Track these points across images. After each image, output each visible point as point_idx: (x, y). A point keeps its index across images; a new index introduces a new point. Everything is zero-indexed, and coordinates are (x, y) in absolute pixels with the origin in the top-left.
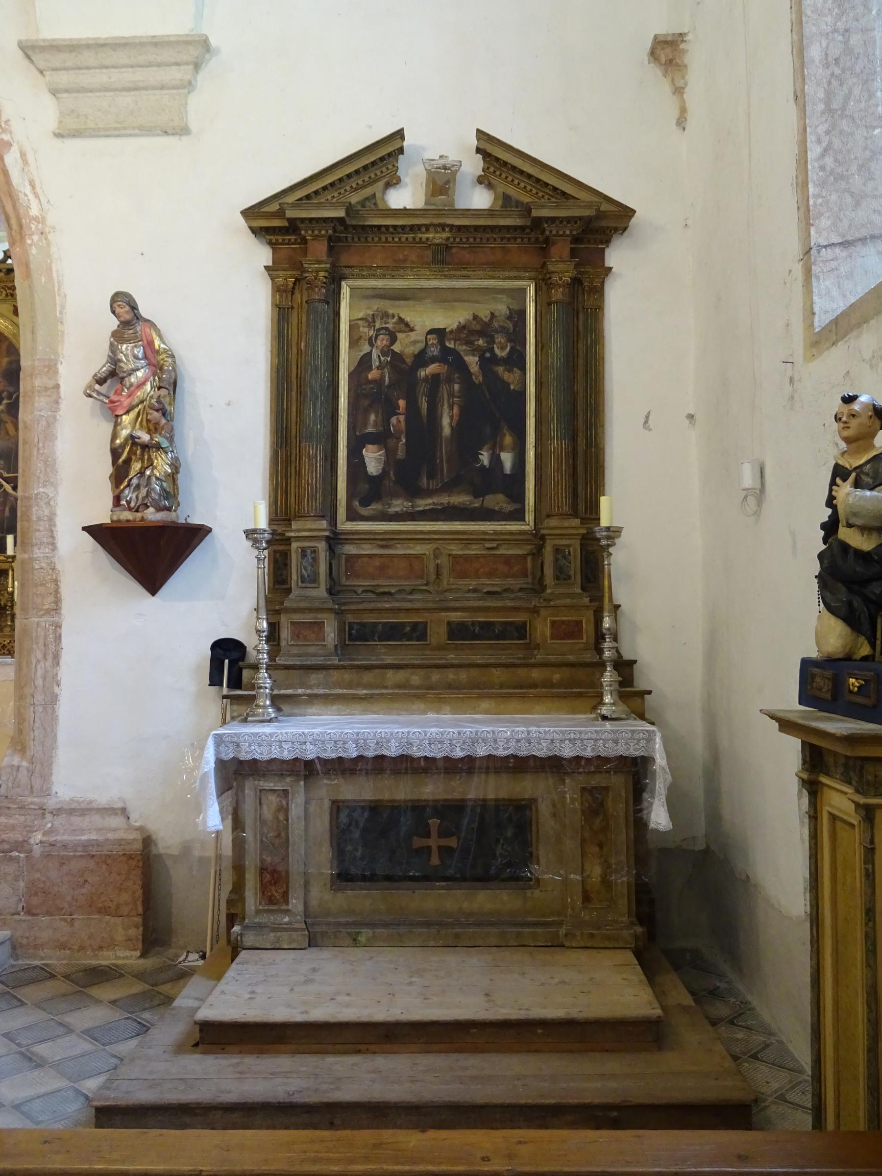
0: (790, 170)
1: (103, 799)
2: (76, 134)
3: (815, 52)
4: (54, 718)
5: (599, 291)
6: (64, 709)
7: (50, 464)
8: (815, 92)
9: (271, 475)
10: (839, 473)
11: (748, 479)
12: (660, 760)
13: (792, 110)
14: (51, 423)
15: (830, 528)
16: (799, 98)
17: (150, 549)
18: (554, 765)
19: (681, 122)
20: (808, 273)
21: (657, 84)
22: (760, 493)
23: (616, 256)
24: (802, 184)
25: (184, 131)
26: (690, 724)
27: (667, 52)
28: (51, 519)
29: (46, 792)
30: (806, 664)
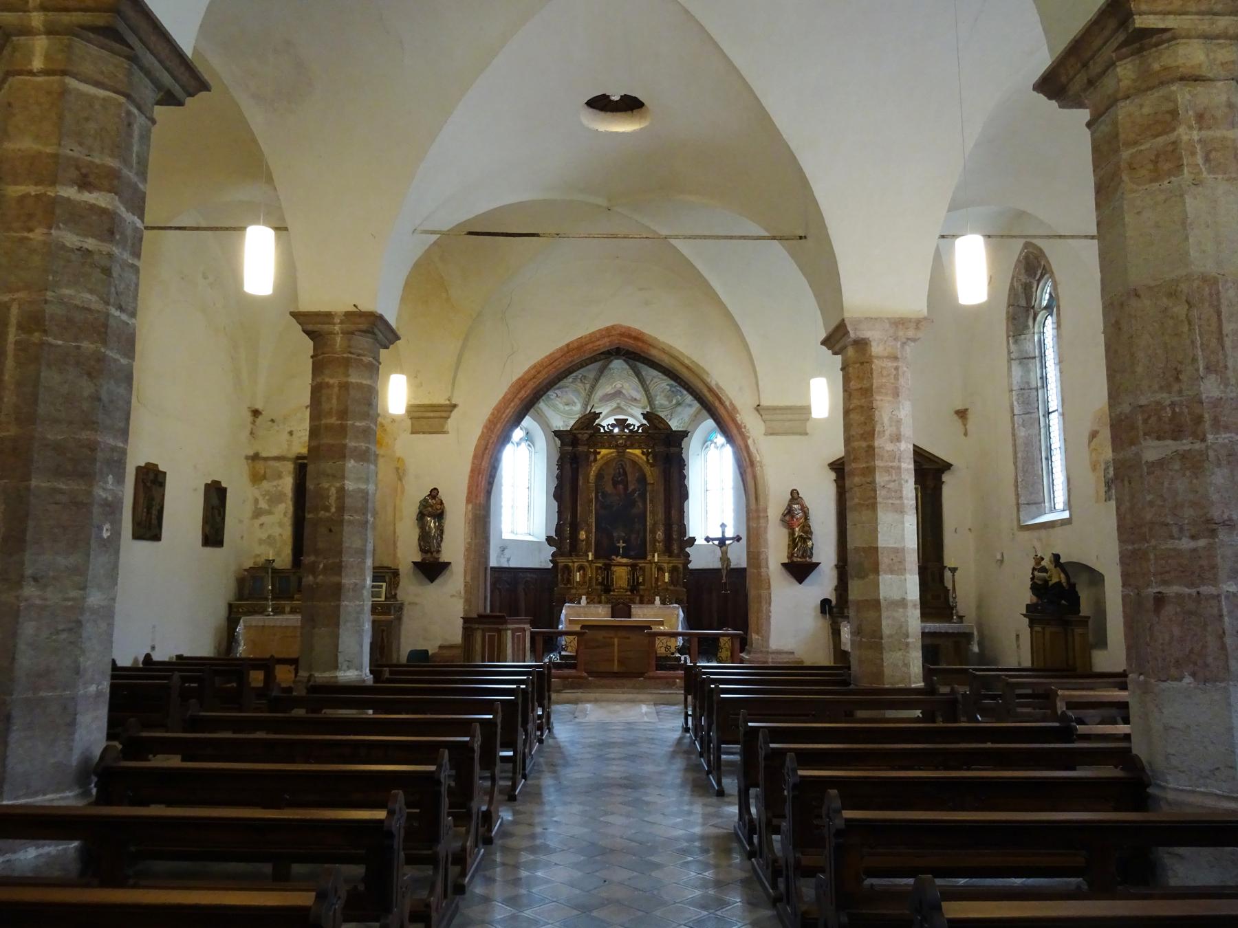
0: (1012, 481)
1: (786, 649)
2: (772, 434)
3: (1019, 455)
4: (769, 623)
5: (941, 489)
6: (773, 621)
7: (766, 541)
8: (1020, 465)
9: (745, 519)
10: (1034, 569)
11: (999, 557)
12: (976, 633)
13: (1013, 467)
14: (766, 528)
15: (1032, 579)
16: (1015, 464)
17: (800, 569)
18: (947, 635)
19: (966, 434)
20: (1018, 510)
21: (957, 422)
22: (1002, 561)
23: (946, 477)
24: (1016, 486)
25: (806, 434)
26: (970, 624)
27: (962, 414)
28: (767, 559)
29: (768, 646)
30: (207, 485)
